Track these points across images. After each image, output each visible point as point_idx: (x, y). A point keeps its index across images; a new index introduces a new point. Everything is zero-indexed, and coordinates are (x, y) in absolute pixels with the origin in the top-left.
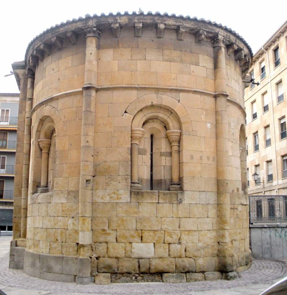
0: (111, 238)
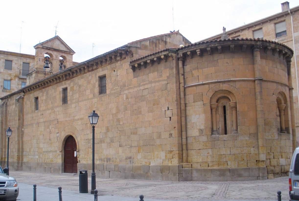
0: (272, 157)
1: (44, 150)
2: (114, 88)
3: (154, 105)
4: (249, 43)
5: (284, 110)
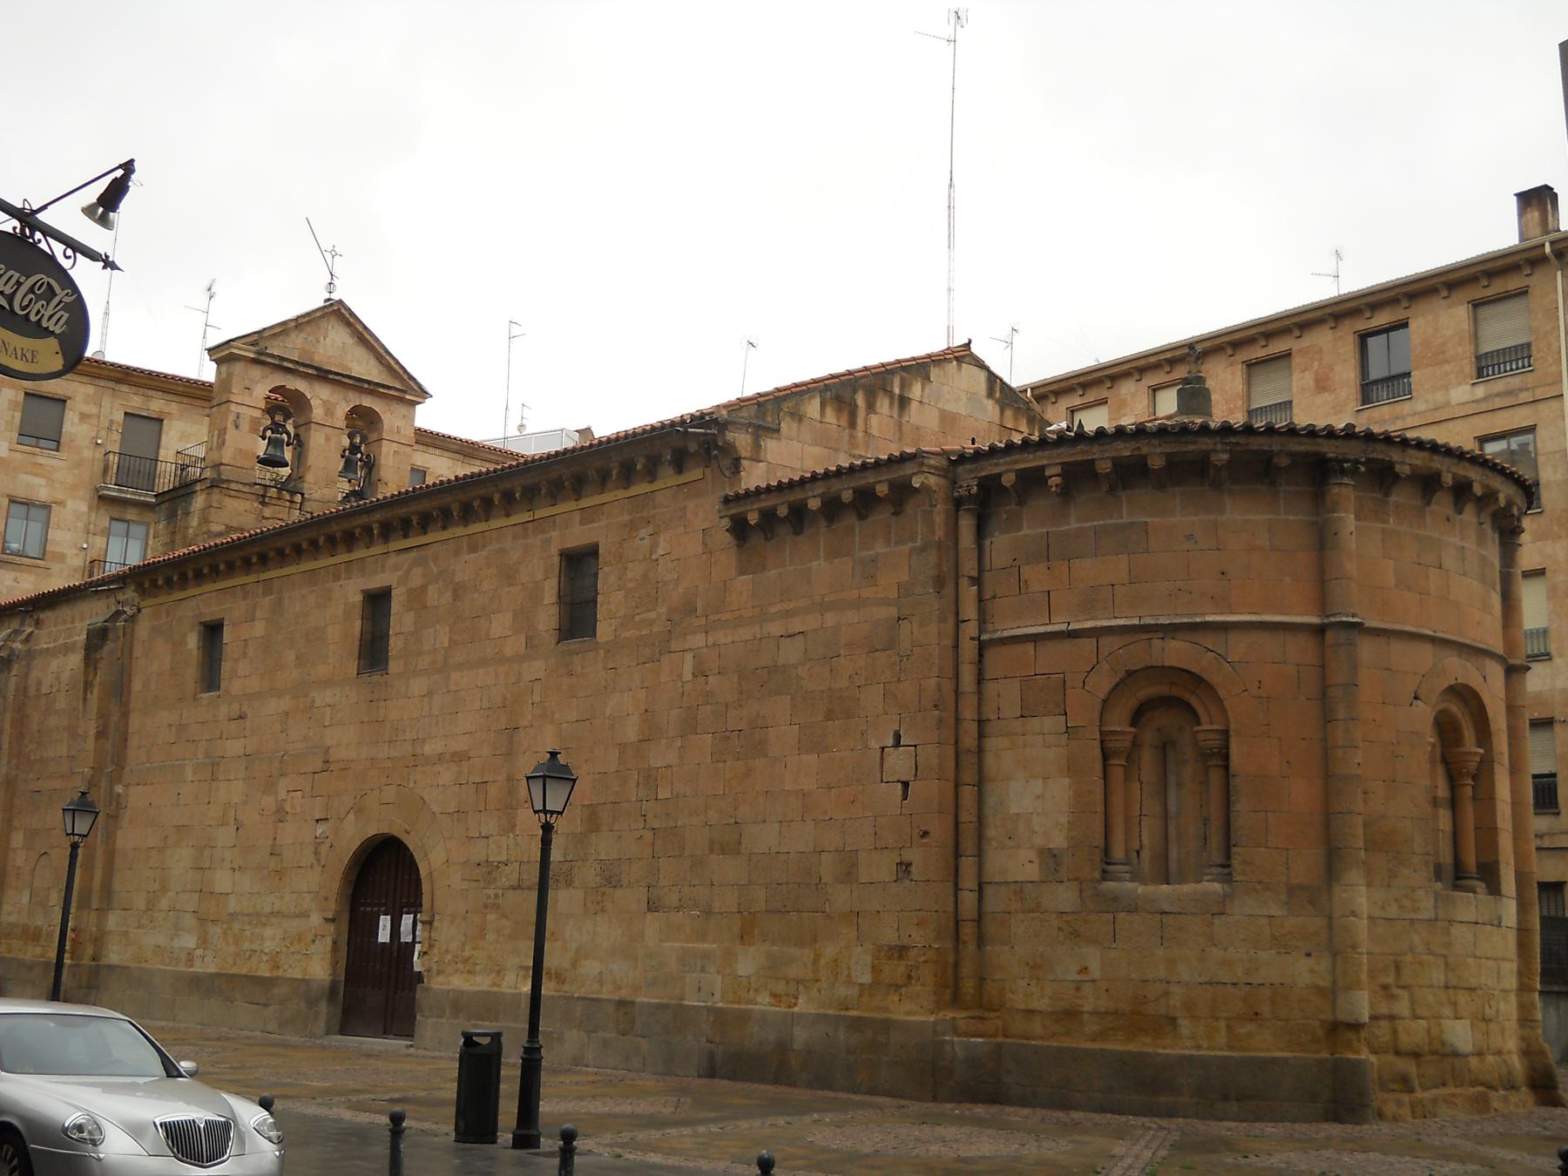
1: (233, 905)
2: (637, 618)
3: (830, 716)
5: (1474, 778)
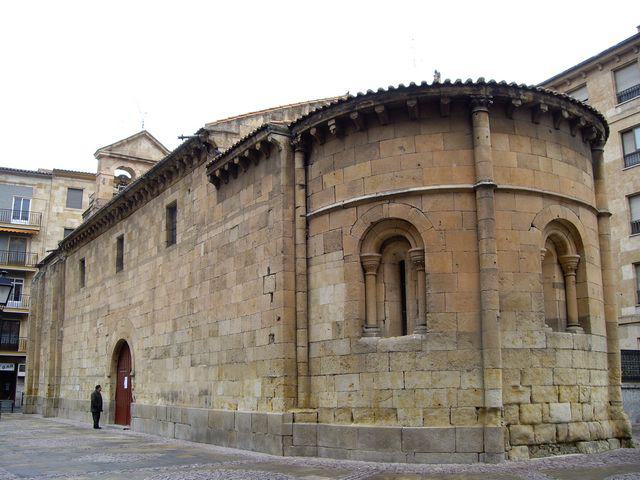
0: (525, 398)
4: (456, 92)
